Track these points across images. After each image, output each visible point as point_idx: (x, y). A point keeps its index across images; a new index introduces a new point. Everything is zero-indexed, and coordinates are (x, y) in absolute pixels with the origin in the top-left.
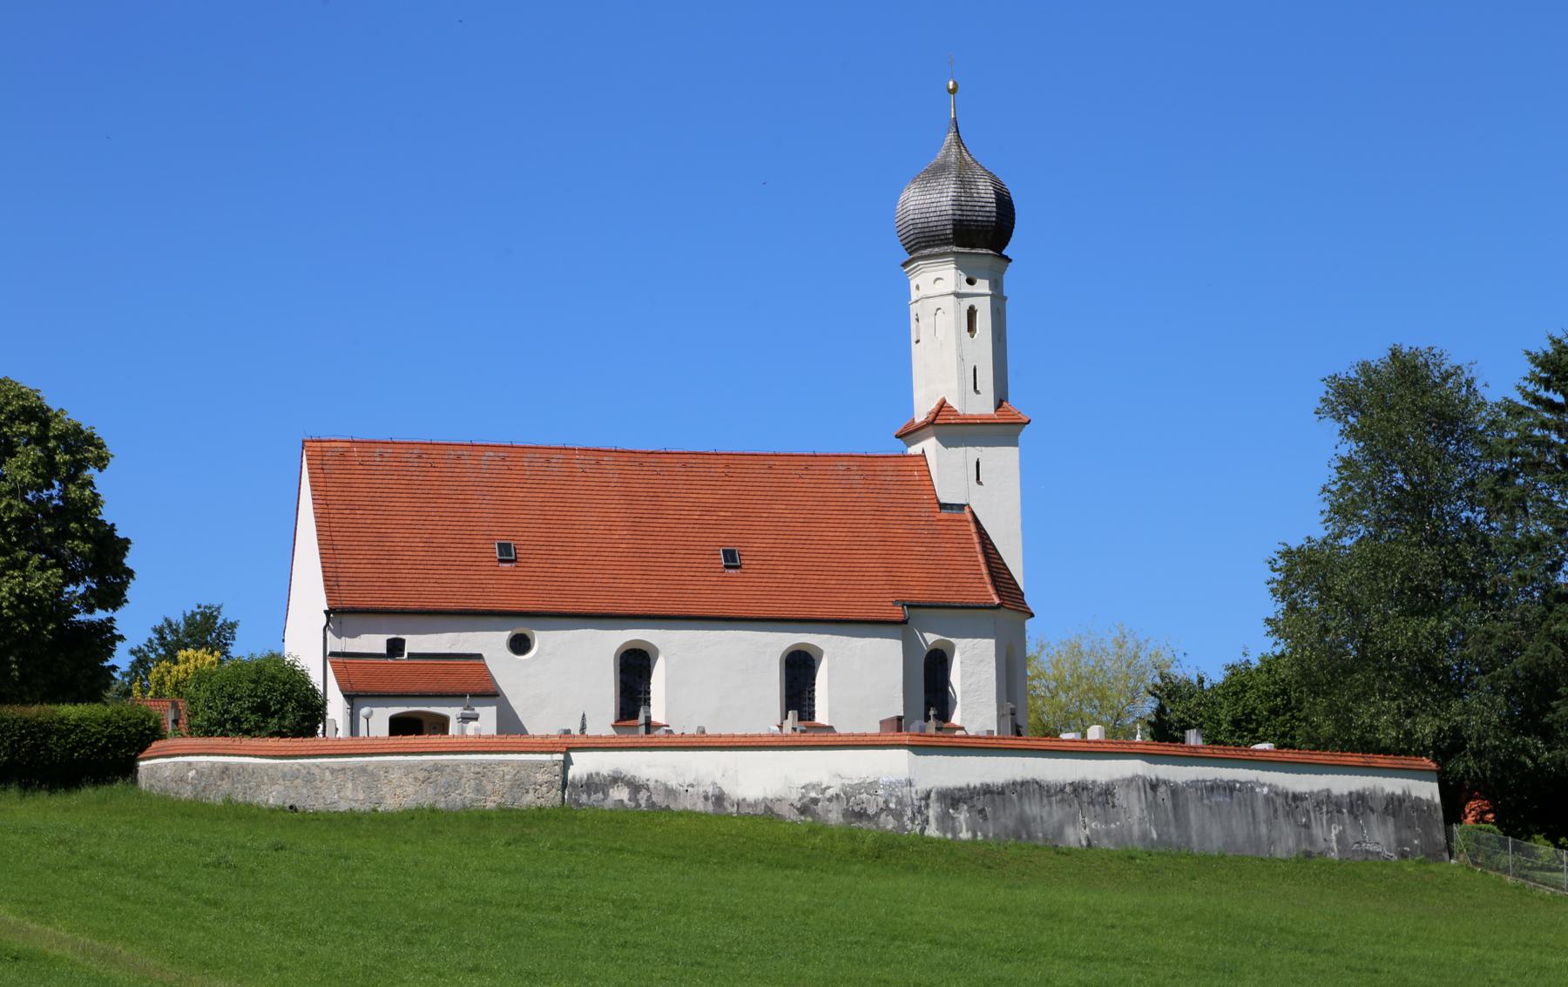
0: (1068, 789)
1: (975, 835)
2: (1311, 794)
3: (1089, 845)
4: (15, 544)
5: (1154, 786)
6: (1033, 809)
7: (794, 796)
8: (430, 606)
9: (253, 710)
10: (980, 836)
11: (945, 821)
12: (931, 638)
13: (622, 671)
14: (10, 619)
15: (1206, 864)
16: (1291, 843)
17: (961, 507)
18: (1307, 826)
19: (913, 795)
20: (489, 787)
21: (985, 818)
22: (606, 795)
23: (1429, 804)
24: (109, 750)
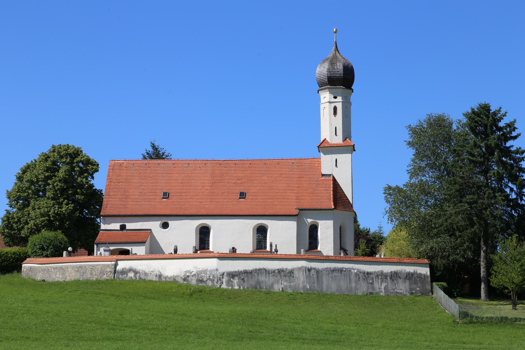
0: (276, 271)
1: (240, 287)
2: (375, 272)
3: (283, 290)
4: (59, 197)
5: (309, 270)
6: (262, 278)
7: (182, 275)
8: (134, 213)
9: (40, 249)
10: (242, 288)
11: (229, 282)
12: (310, 220)
13: (200, 234)
14: (53, 221)
15: (331, 297)
16: (365, 289)
17: (330, 175)
18: (372, 284)
19: (218, 274)
20: (94, 273)
21: (244, 282)
22: (127, 275)
23: (425, 276)
24: (13, 262)
